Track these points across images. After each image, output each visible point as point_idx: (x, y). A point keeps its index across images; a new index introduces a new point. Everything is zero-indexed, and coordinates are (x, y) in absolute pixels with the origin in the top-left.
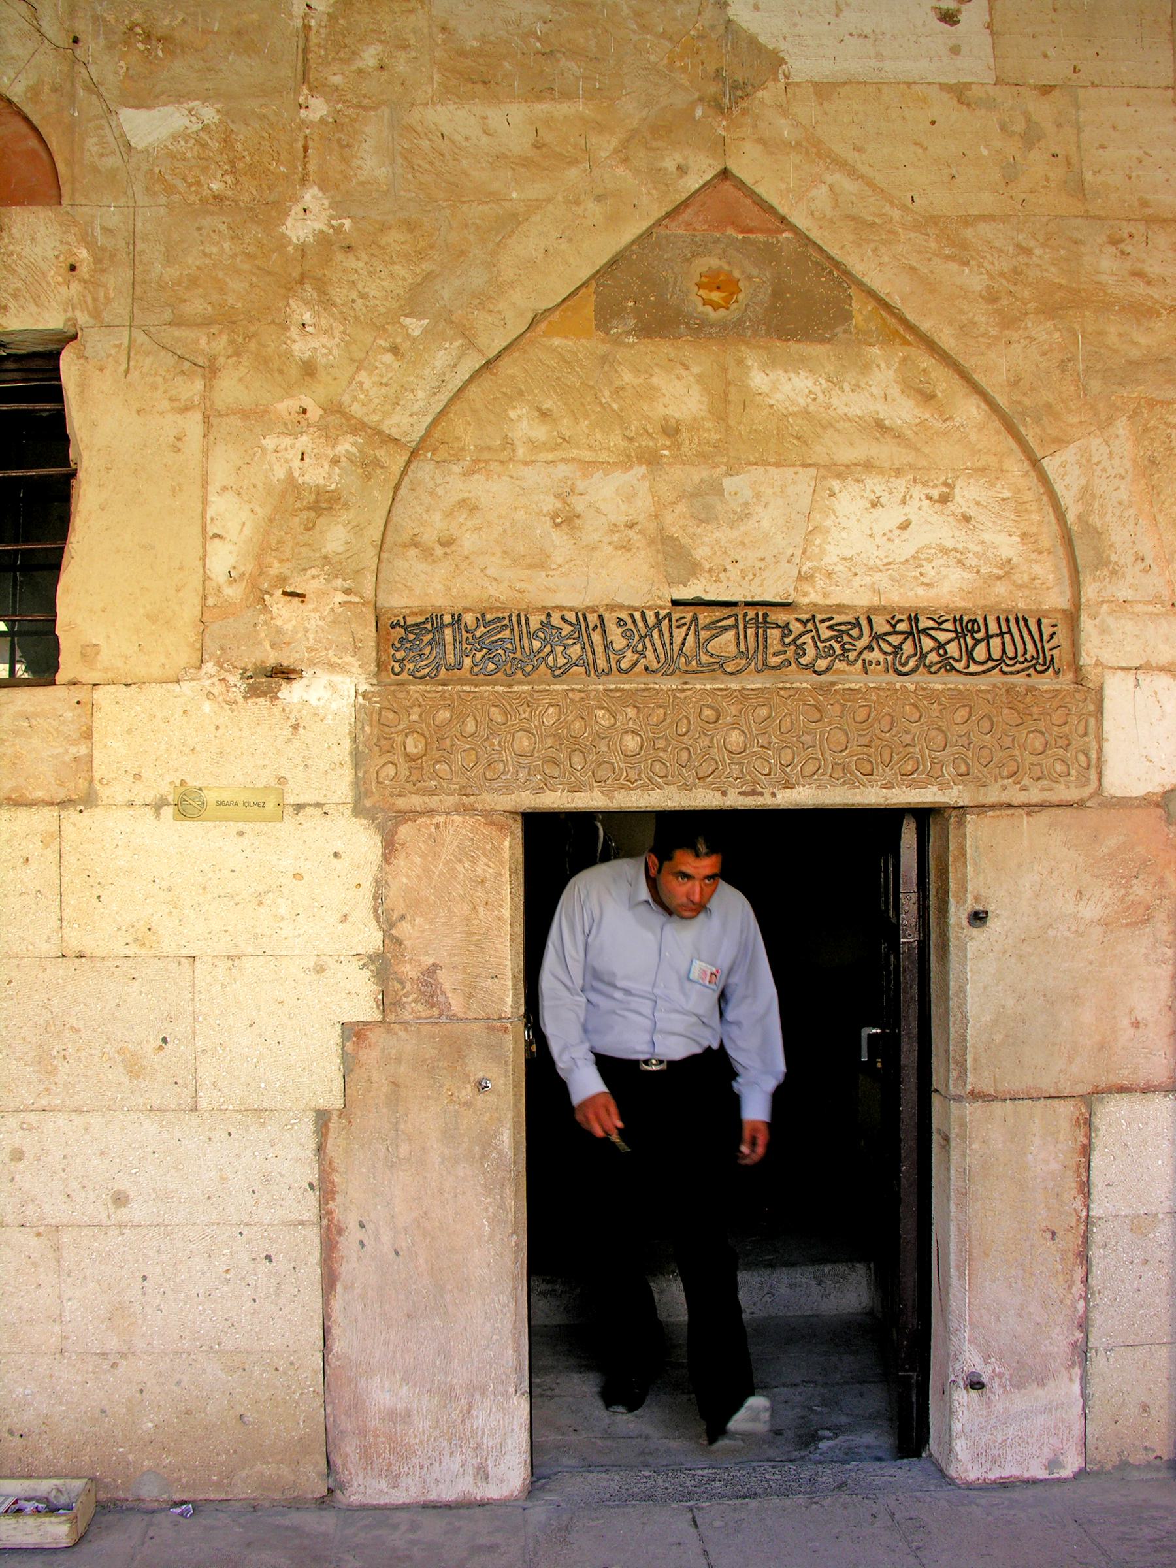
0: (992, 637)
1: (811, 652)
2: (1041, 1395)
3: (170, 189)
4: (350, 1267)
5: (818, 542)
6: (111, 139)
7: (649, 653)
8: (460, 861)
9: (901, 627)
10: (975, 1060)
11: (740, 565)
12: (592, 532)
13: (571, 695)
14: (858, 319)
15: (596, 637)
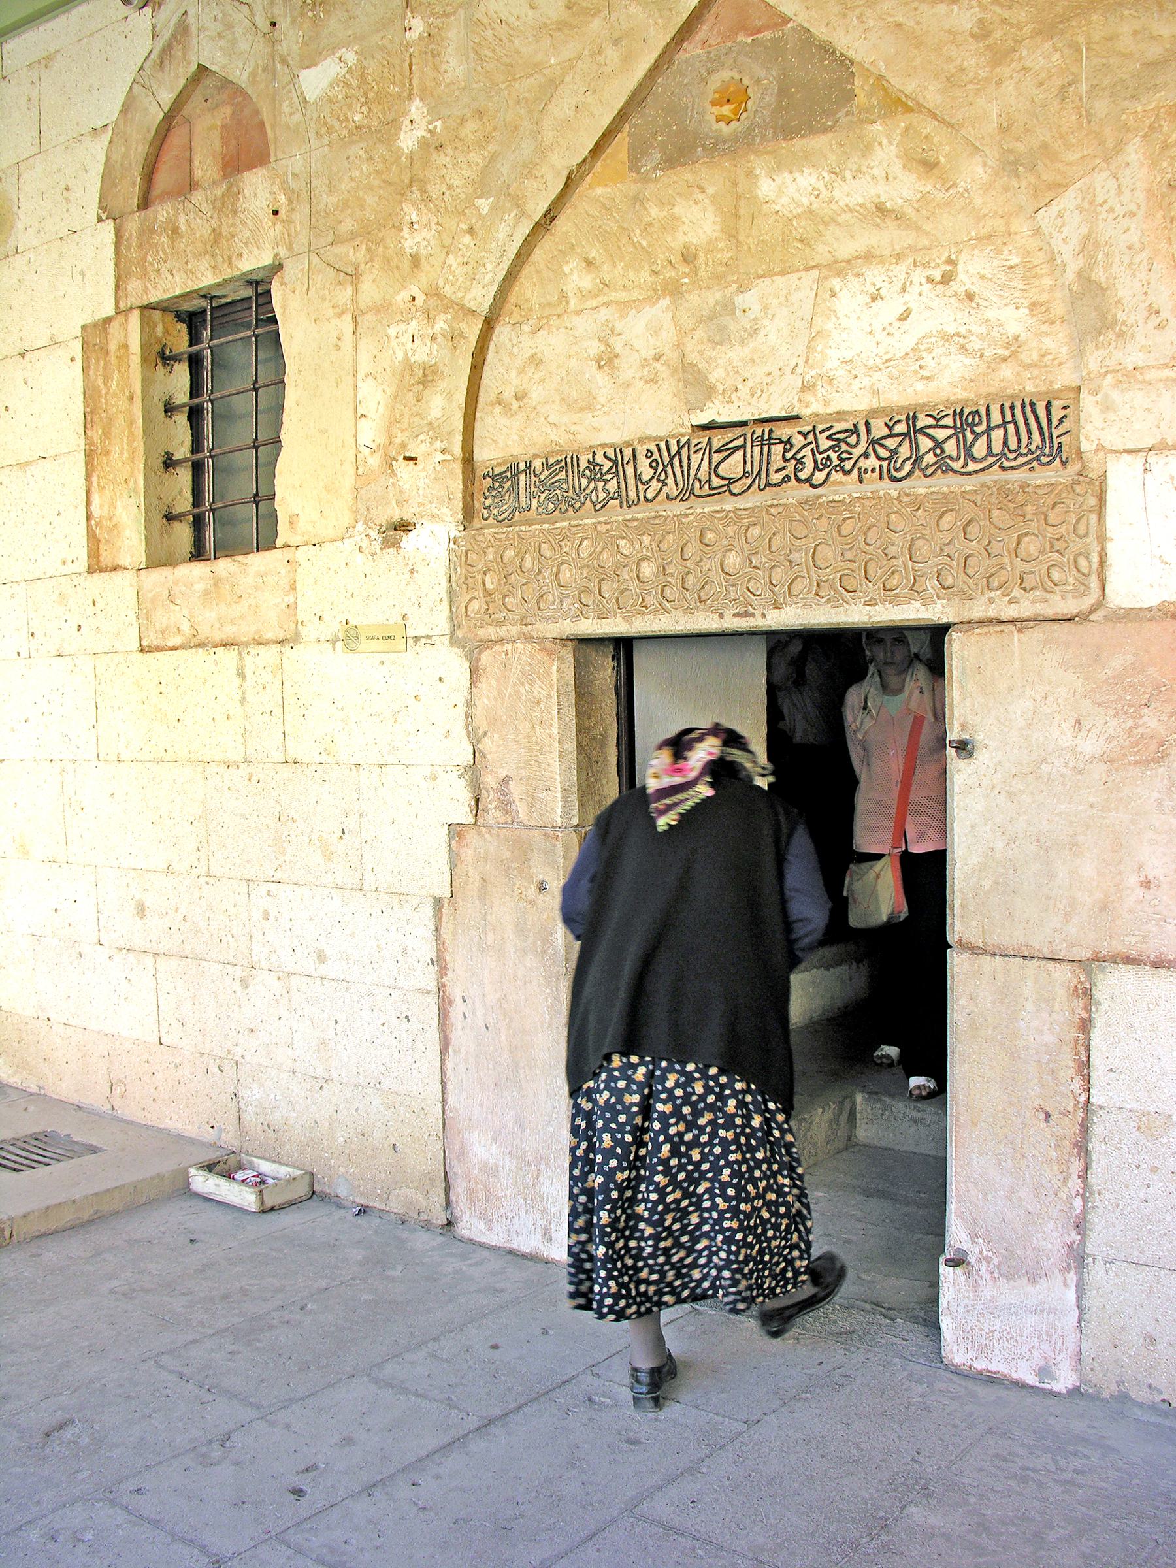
0: (993, 429)
1: (809, 464)
2: (1033, 1293)
3: (330, 129)
4: (458, 1035)
5: (819, 349)
6: (296, 99)
7: (670, 481)
8: (523, 684)
9: (901, 428)
10: (963, 907)
11: (749, 383)
12: (628, 368)
13: (599, 527)
14: (861, 98)
15: (629, 470)
